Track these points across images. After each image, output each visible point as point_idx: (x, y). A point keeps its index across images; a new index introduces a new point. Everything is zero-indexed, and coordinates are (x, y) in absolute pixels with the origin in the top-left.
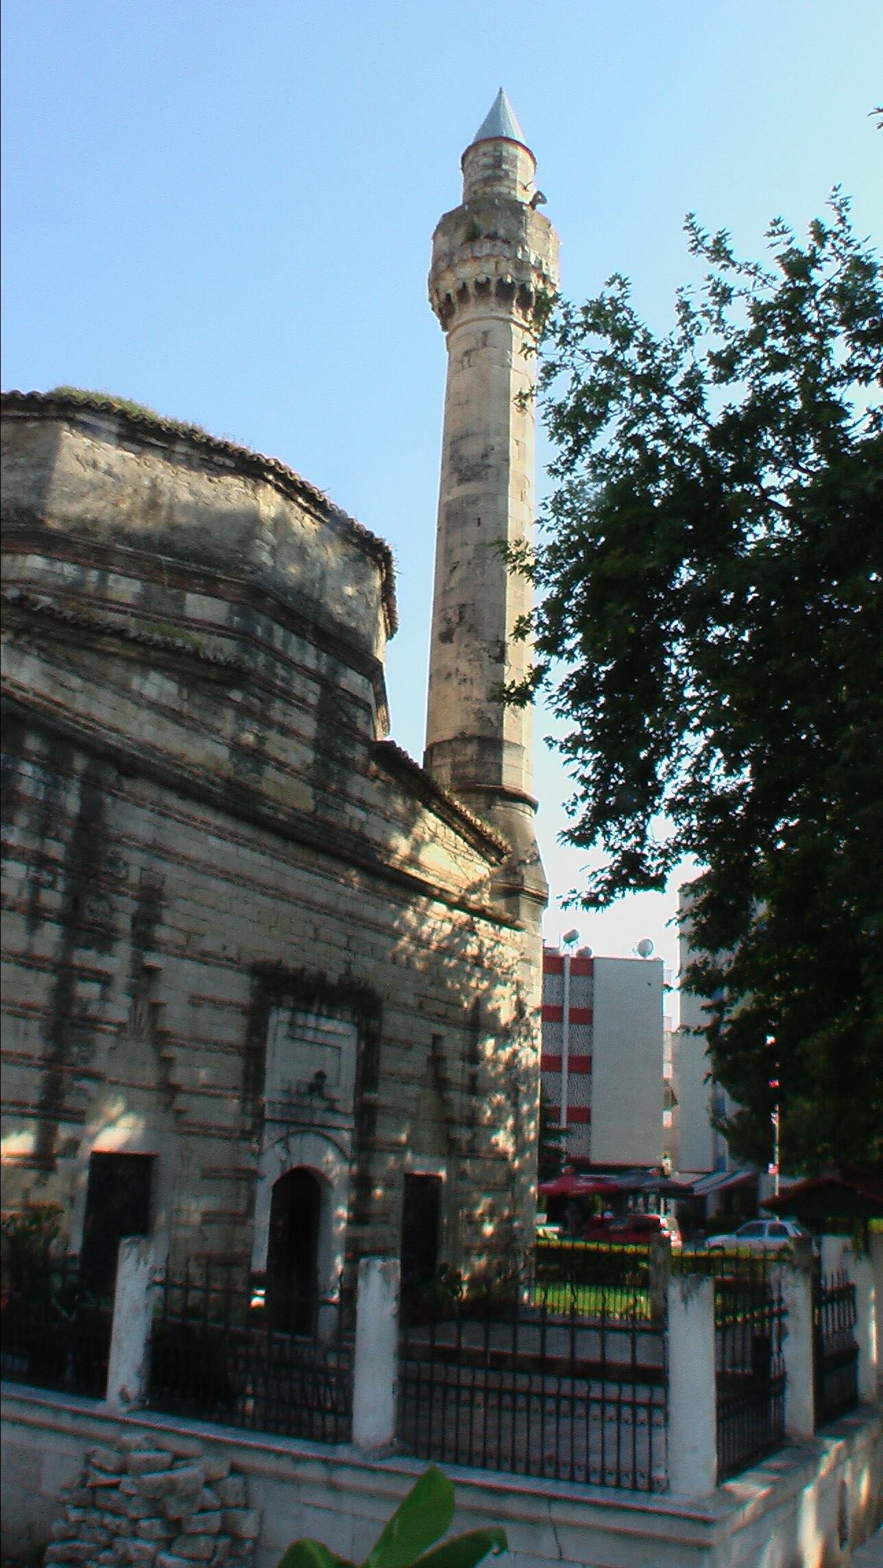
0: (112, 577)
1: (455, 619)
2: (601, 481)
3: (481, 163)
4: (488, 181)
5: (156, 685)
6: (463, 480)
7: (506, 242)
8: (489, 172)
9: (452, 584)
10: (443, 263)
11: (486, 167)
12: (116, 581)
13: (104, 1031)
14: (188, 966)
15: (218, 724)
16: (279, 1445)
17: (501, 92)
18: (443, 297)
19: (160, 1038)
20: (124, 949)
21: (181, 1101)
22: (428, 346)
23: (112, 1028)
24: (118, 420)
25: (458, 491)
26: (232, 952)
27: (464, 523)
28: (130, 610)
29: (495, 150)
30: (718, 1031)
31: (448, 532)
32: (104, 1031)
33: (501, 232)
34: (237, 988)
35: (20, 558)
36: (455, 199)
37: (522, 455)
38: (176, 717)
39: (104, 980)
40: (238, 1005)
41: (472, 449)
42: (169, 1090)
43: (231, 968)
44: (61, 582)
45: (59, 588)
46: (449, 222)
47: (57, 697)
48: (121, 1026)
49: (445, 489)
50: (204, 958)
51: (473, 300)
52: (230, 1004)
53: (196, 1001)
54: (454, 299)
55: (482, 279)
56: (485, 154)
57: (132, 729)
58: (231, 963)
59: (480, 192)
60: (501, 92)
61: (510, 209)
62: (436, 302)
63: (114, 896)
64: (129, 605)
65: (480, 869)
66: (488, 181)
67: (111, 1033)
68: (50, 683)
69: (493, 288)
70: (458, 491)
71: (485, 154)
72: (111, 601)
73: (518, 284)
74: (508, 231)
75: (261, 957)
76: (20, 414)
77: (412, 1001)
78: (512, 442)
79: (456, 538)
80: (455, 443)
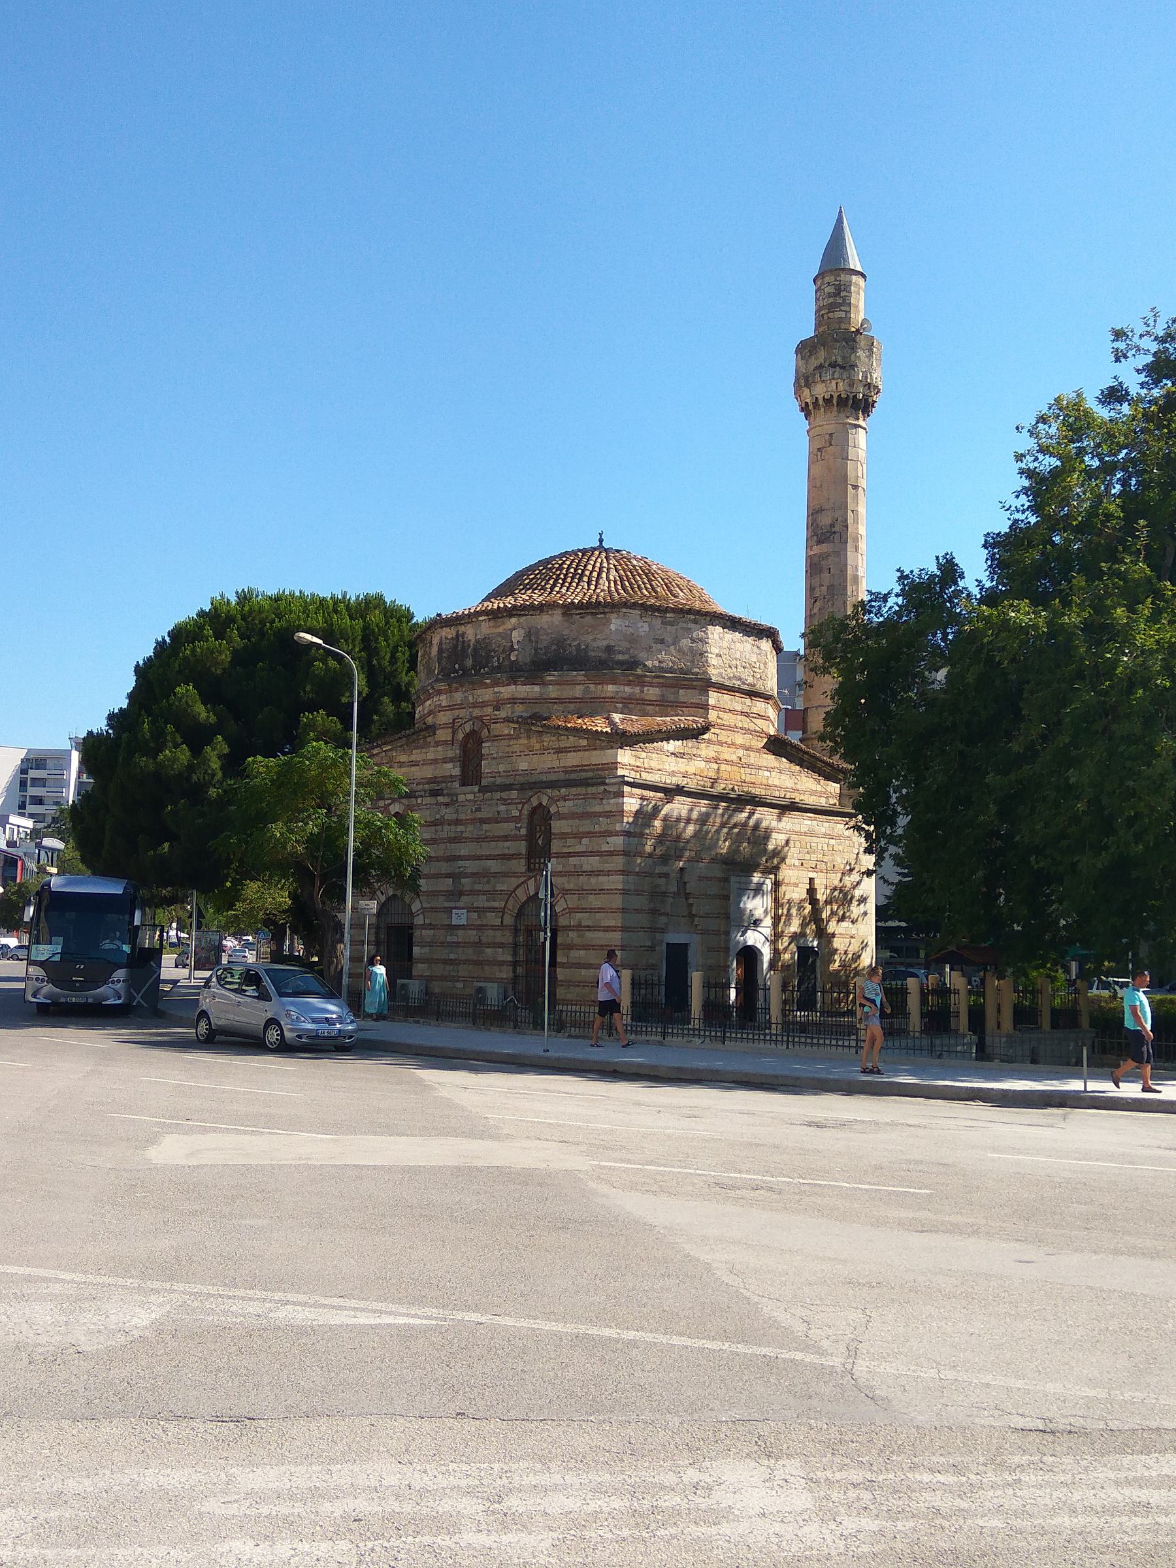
2: (774, 850)
4: (831, 307)
5: (673, 745)
6: (819, 542)
8: (831, 300)
9: (816, 611)
10: (803, 381)
11: (829, 295)
17: (841, 212)
19: (687, 896)
22: (793, 434)
25: (817, 550)
27: (821, 572)
30: (191, 749)
33: (840, 360)
36: (809, 332)
37: (856, 521)
38: (682, 755)
41: (825, 520)
42: (692, 916)
46: (805, 349)
49: (809, 547)
60: (841, 212)
66: (831, 307)
70: (817, 550)
74: (844, 358)
77: (797, 863)
78: (850, 512)
79: (816, 582)
80: (814, 513)
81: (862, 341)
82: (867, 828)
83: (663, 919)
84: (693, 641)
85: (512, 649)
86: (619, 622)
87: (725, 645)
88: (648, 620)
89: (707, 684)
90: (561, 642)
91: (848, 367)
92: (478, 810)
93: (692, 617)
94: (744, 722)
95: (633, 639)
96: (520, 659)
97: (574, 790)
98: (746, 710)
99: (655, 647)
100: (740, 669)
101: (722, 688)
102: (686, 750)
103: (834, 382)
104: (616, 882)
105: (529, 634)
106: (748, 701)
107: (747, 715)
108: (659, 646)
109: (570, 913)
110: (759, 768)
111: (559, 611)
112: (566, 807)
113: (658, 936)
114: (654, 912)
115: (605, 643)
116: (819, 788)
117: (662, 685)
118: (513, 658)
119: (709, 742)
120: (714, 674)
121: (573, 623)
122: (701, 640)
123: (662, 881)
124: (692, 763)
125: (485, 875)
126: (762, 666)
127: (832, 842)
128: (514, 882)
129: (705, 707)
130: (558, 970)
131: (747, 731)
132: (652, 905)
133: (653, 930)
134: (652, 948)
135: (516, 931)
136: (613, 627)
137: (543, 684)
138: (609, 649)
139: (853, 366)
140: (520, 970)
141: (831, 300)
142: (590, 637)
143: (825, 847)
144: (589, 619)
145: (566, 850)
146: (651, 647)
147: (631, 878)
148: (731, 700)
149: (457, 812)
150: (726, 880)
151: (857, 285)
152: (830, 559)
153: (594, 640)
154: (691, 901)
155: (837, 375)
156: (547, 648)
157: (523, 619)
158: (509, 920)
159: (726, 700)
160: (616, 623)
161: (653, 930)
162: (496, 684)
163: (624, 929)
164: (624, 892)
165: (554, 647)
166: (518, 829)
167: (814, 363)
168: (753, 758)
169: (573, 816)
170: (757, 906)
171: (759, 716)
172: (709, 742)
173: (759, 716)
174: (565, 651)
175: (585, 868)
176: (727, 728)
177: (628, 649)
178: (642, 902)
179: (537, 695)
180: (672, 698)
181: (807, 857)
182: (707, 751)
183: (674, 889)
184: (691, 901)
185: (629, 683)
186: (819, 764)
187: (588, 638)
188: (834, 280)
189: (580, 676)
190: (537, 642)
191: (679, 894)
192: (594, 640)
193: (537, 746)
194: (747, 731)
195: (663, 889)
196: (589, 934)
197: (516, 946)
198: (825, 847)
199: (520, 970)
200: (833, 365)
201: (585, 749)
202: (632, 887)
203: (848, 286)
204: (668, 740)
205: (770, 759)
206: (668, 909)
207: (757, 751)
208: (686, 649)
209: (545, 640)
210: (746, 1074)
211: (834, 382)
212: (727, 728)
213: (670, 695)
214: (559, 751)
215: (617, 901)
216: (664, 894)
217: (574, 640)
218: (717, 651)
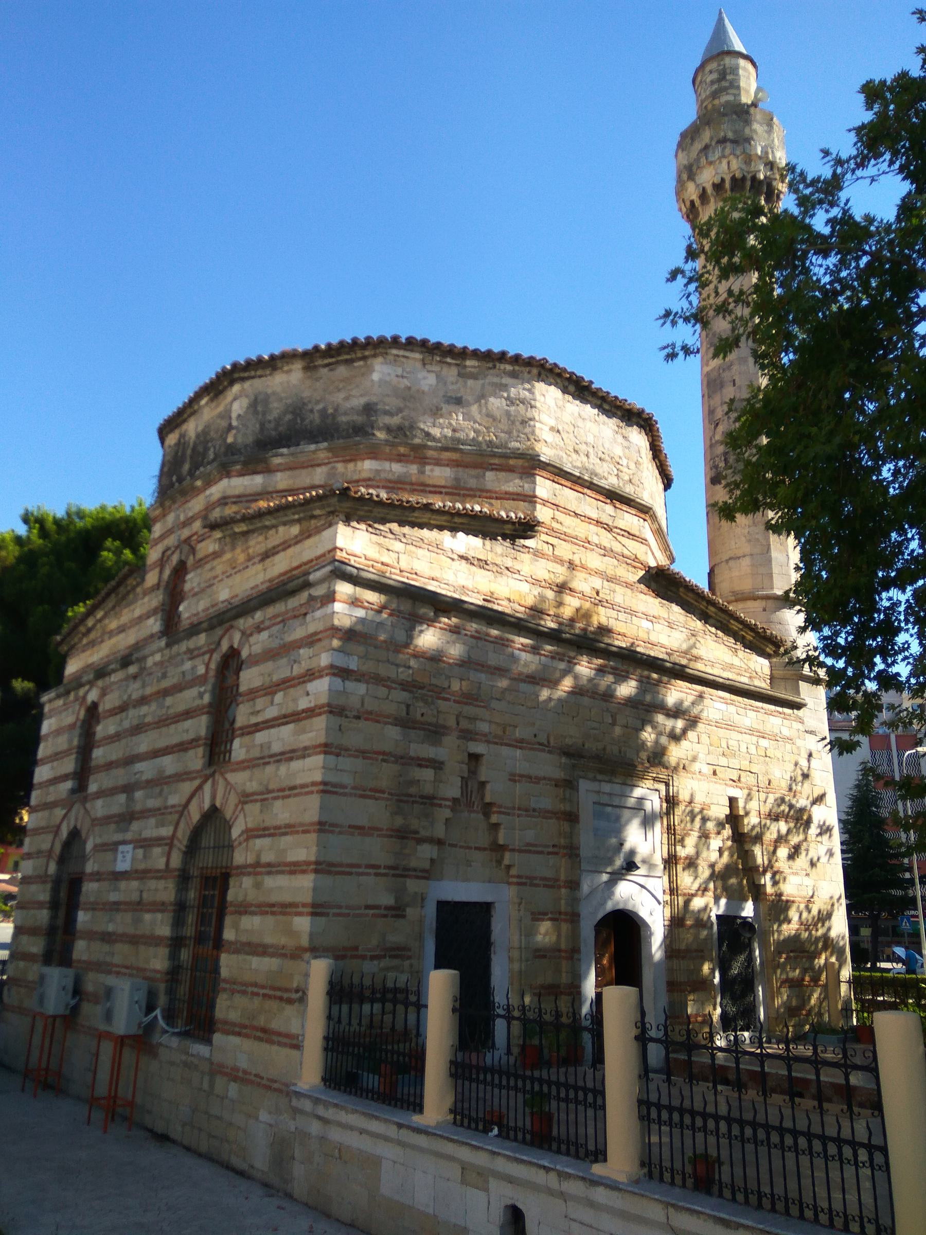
0: (428, 468)
1: (722, 465)
3: (708, 80)
5: (465, 543)
7: (735, 142)
8: (716, 86)
11: (712, 82)
12: (432, 470)
13: (440, 806)
14: (505, 751)
15: (517, 566)
16: (375, 1126)
17: (720, 13)
18: (688, 204)
20: (451, 741)
21: (507, 858)
23: (448, 803)
24: (420, 349)
26: (542, 738)
28: (444, 490)
29: (719, 65)
31: (709, 397)
32: (440, 806)
33: (730, 135)
34: (549, 766)
35: (359, 464)
36: (689, 114)
38: (483, 564)
39: (437, 765)
40: (550, 779)
42: (498, 849)
43: (543, 751)
44: (390, 477)
45: (390, 481)
46: (689, 136)
47: (385, 559)
48: (455, 800)
50: (519, 744)
51: (712, 200)
52: (545, 778)
53: (514, 778)
54: (697, 203)
55: (717, 180)
56: (711, 72)
57: (449, 576)
58: (544, 746)
59: (710, 107)
61: (736, 113)
62: (684, 210)
63: (440, 701)
64: (444, 487)
65: (761, 665)
67: (448, 807)
68: (377, 548)
69: (727, 185)
71: (711, 72)
72: (428, 485)
73: (749, 177)
74: (735, 132)
75: (568, 741)
76: (348, 357)
77: (707, 770)
81: (757, 115)
82: (829, 661)
83: (427, 851)
84: (511, 401)
85: (230, 427)
86: (386, 369)
87: (567, 418)
88: (436, 368)
89: (531, 465)
90: (298, 409)
91: (742, 141)
92: (164, 676)
93: (509, 367)
94: (605, 539)
95: (410, 396)
96: (240, 440)
97: (271, 611)
98: (605, 519)
99: (445, 408)
100: (594, 459)
101: (559, 473)
102: (490, 557)
103: (725, 162)
104: (311, 769)
105: (254, 405)
106: (609, 509)
107: (609, 529)
108: (452, 407)
109: (247, 840)
110: (632, 613)
111: (298, 366)
112: (260, 642)
113: (413, 886)
114: (403, 835)
115: (363, 401)
116: (736, 661)
117: (456, 464)
118: (230, 440)
119: (538, 554)
120: (546, 453)
121: (317, 380)
122: (523, 402)
123: (428, 774)
124: (503, 580)
125: (160, 782)
126: (632, 466)
127: (764, 743)
128: (187, 787)
129: (531, 499)
130: (224, 957)
131: (607, 552)
132: (399, 821)
133: (399, 872)
134: (397, 911)
135: (184, 878)
136: (376, 376)
137: (269, 470)
138: (369, 409)
139: (748, 140)
140: (185, 955)
141: (716, 86)
142: (342, 395)
143: (753, 750)
144: (342, 371)
145: (259, 719)
146: (438, 409)
147: (346, 763)
148: (578, 499)
149: (143, 686)
150: (569, 784)
151: (745, 69)
152: (735, 368)
153: (347, 398)
154: (494, 819)
155: (727, 151)
156: (278, 421)
157: (247, 384)
158: (176, 861)
159: (568, 496)
160: (380, 371)
161: (399, 872)
162: (208, 484)
163: (322, 867)
164: (327, 789)
165: (289, 417)
166: (201, 696)
167: (698, 146)
168: (620, 596)
169: (271, 655)
170: (642, 841)
171: (631, 535)
172: (538, 554)
173: (631, 535)
174: (303, 420)
175: (276, 748)
176: (565, 537)
177: (400, 410)
178: (374, 812)
179: (259, 489)
180: (472, 483)
181: (723, 761)
182: (526, 564)
183: (452, 789)
184: (494, 819)
185: (400, 458)
186: (735, 626)
187: (339, 397)
188: (718, 65)
189: (319, 450)
190: (264, 414)
191: (470, 805)
192: (347, 398)
193: (241, 558)
194: (607, 552)
195: (428, 789)
196: (270, 882)
197: (180, 908)
198: (753, 750)
199: (185, 955)
200: (723, 141)
201: (298, 540)
202: (347, 780)
203: (735, 70)
204: (454, 529)
205: (651, 603)
206: (440, 831)
207: (628, 585)
208: (497, 414)
209: (276, 409)
210: (616, 1181)
211: (725, 162)
212: (565, 537)
213: (469, 479)
214: (266, 555)
215: (309, 809)
216: (430, 801)
217: (318, 402)
218: (552, 423)
